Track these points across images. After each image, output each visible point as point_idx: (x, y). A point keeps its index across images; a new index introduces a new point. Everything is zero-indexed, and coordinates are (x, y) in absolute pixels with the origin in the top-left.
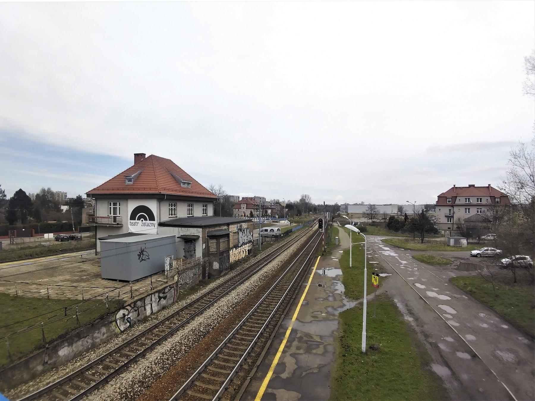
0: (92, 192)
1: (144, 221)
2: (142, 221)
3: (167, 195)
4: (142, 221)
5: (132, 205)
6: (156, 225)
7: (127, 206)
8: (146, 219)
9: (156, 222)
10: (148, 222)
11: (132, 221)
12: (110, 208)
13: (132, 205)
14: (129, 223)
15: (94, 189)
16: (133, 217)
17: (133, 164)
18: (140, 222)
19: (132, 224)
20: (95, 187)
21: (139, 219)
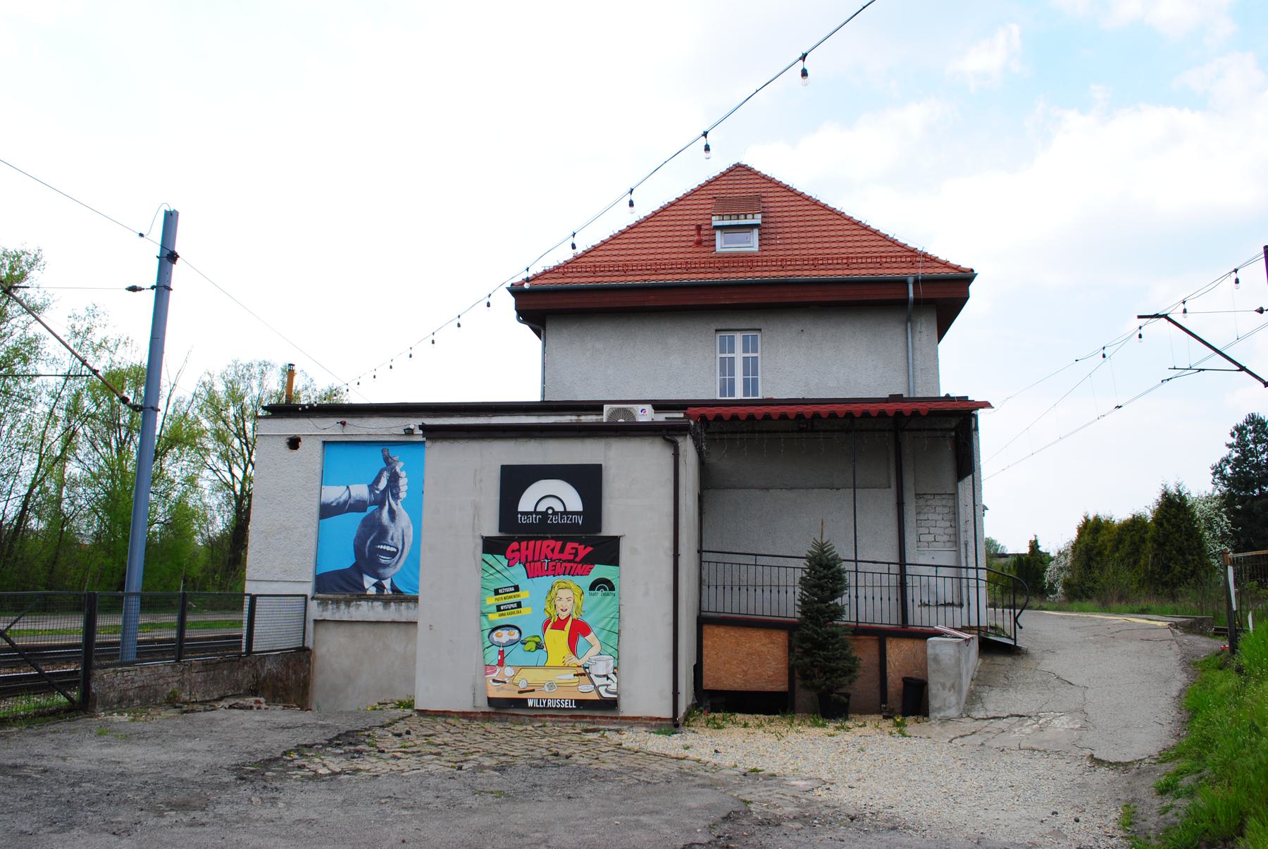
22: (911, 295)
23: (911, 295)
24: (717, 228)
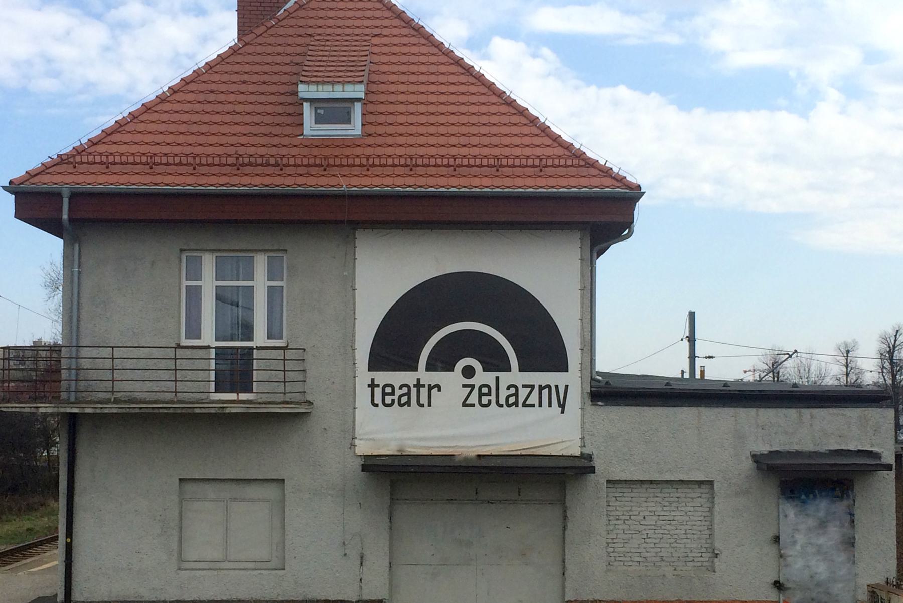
0: (65, 182)
1: (482, 377)
2: (468, 372)
3: (77, 196)
4: (468, 372)
5: (385, 274)
6: (575, 400)
7: (349, 285)
8: (495, 361)
9: (572, 379)
10: (515, 376)
11: (383, 377)
12: (194, 295)
13: (385, 274)
14: (363, 394)
15: (63, 160)
16: (395, 345)
17: (62, 241)
18: (451, 381)
19: (387, 397)
20: (65, 146)
21: (442, 360)
22: (65, 217)
23: (65, 217)
24: (311, 101)
